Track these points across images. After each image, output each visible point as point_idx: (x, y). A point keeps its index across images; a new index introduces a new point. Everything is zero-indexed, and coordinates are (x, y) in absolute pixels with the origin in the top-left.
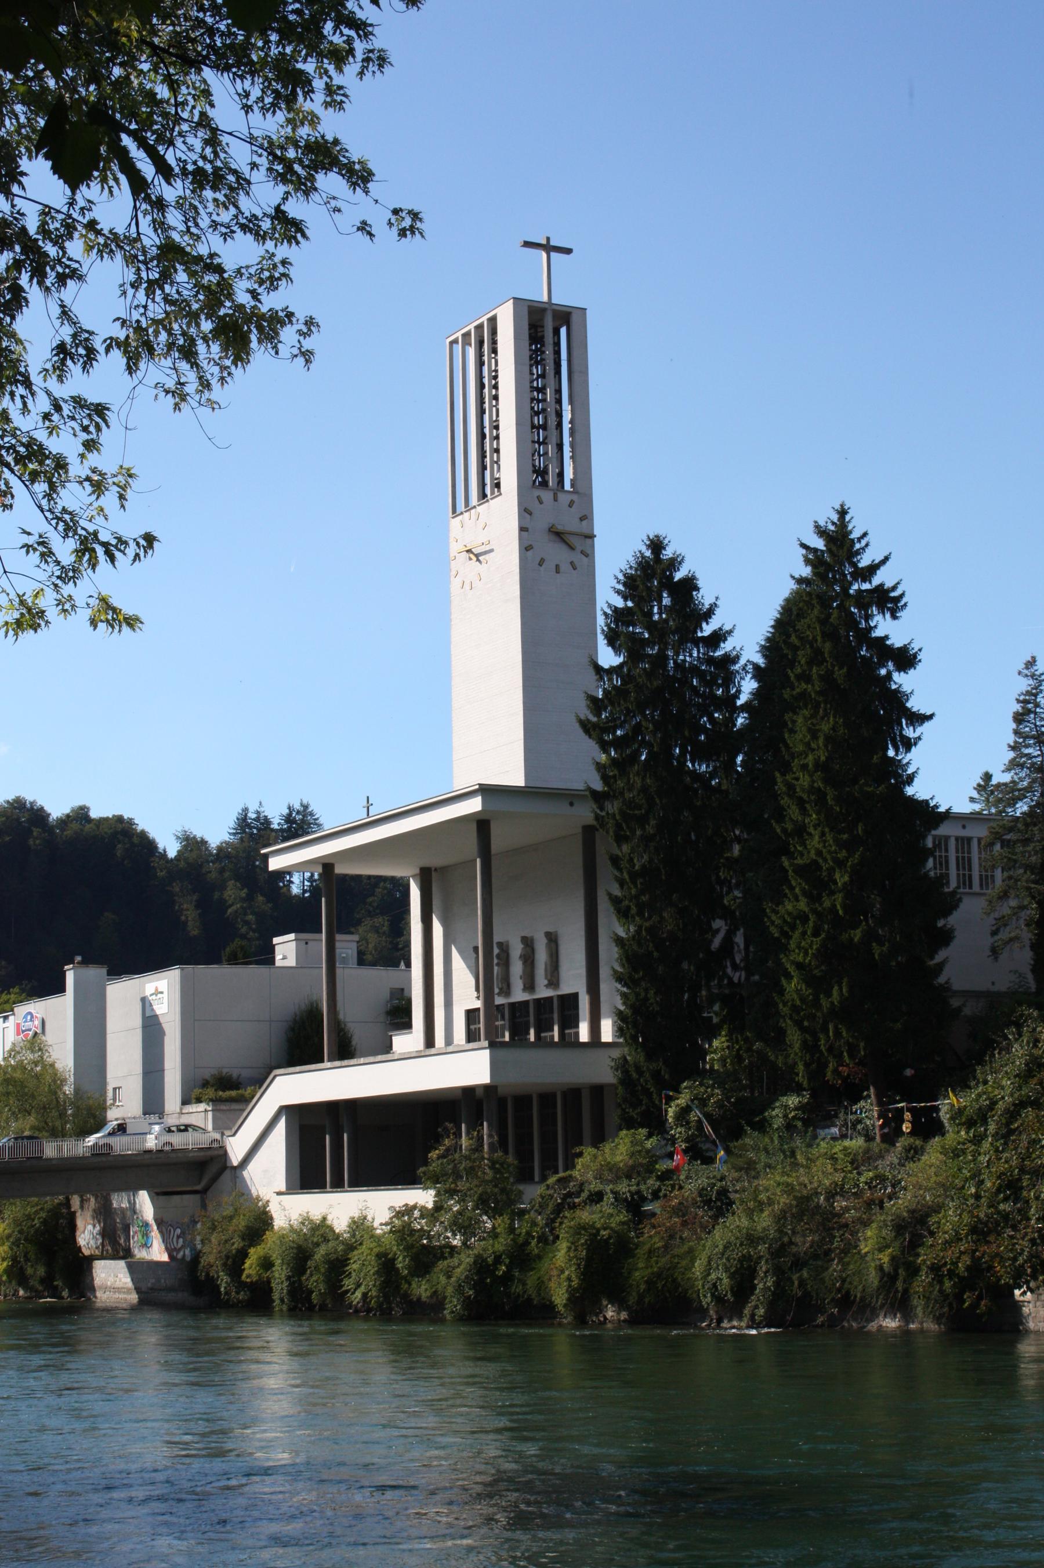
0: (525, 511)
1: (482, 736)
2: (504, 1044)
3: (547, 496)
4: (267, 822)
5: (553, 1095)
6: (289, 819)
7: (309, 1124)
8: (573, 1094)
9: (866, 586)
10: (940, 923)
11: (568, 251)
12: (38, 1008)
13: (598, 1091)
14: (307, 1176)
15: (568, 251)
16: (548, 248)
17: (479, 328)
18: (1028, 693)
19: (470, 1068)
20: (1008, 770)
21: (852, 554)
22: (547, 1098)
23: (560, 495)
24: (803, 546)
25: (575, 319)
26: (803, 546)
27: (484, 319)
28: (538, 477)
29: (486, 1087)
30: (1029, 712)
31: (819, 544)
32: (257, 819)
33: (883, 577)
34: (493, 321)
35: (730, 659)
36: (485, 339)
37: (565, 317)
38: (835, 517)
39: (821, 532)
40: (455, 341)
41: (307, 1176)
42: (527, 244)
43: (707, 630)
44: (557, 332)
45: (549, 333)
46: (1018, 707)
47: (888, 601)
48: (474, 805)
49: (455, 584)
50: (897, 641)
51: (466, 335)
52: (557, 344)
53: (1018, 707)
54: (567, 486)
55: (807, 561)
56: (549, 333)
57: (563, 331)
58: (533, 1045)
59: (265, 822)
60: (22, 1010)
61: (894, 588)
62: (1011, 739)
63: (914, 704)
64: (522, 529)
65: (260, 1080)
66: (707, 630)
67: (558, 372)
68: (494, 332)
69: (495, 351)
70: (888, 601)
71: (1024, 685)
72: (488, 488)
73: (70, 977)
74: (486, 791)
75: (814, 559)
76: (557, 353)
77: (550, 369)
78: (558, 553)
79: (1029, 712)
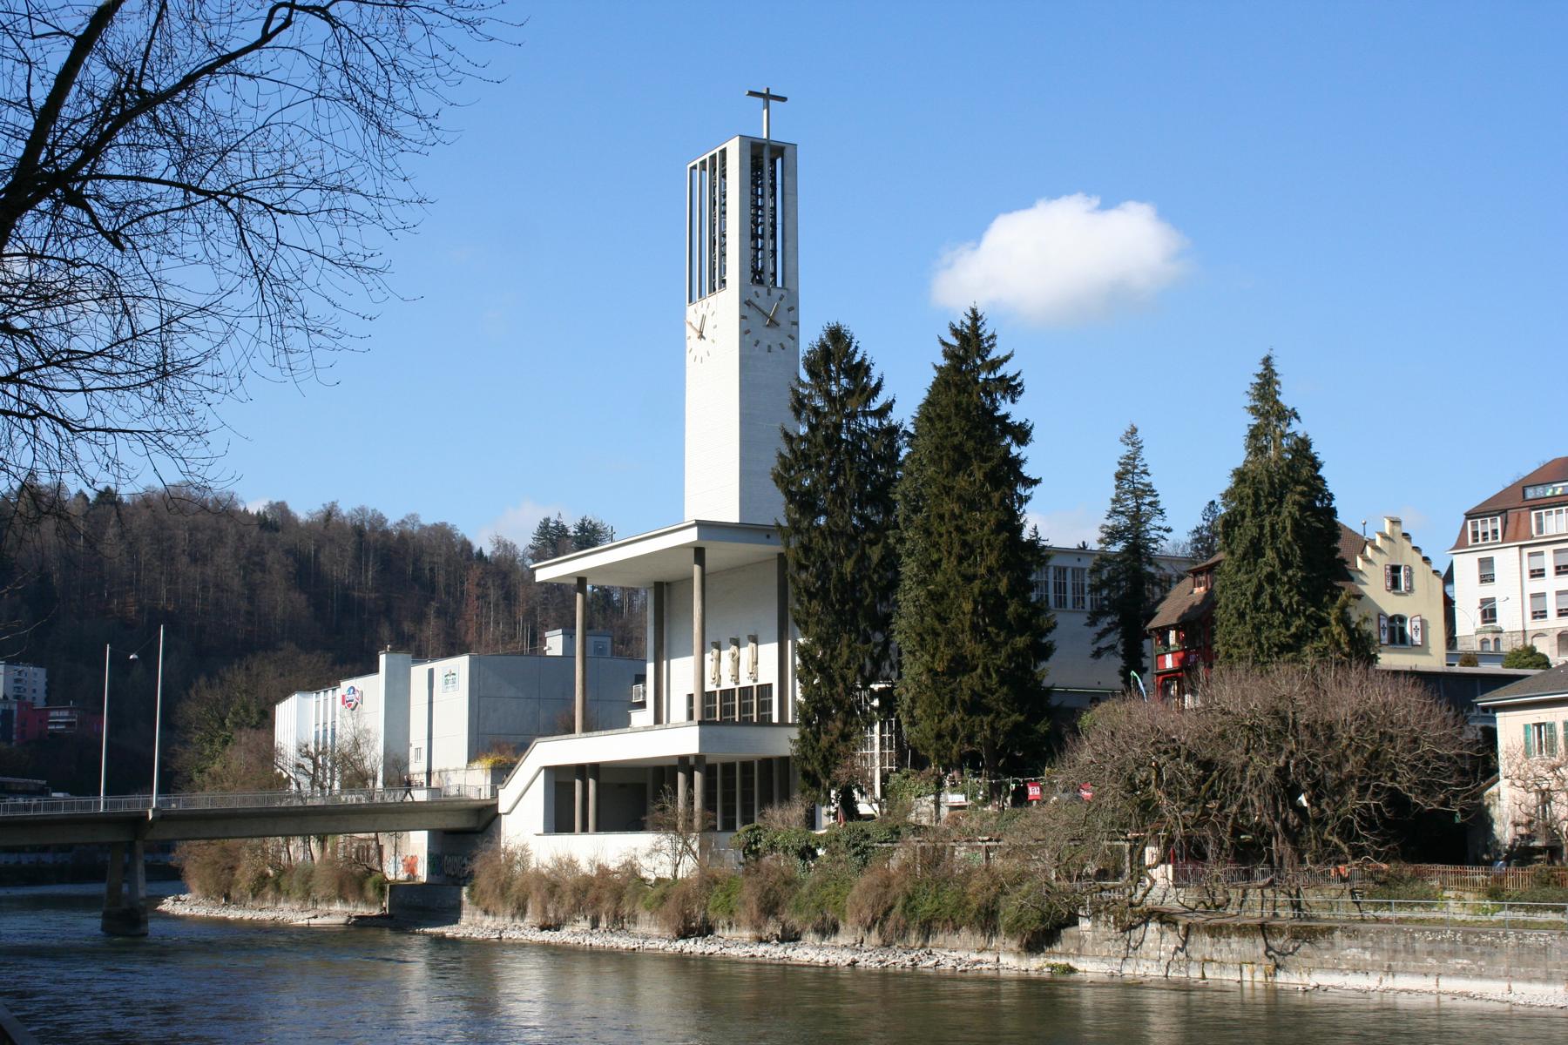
0: (746, 303)
1: (711, 476)
2: (714, 723)
3: (762, 290)
4: (564, 529)
5: (752, 763)
6: (582, 528)
7: (561, 781)
8: (767, 763)
9: (992, 376)
10: (1044, 641)
11: (784, 99)
12: (359, 683)
13: (785, 760)
14: (560, 820)
15: (784, 99)
16: (767, 97)
17: (713, 157)
18: (1128, 457)
19: (682, 740)
20: (1110, 516)
21: (982, 352)
22: (747, 766)
23: (774, 291)
24: (944, 343)
25: (787, 153)
26: (944, 343)
27: (717, 151)
28: (756, 275)
29: (696, 756)
30: (1128, 472)
31: (954, 342)
32: (556, 528)
33: (1007, 370)
34: (723, 152)
35: (892, 431)
36: (717, 165)
37: (779, 150)
38: (968, 322)
39: (956, 333)
40: (695, 167)
41: (560, 820)
42: (752, 93)
43: (875, 405)
44: (773, 162)
45: (766, 162)
46: (1119, 468)
47: (1011, 388)
48: (691, 536)
49: (689, 358)
50: (1016, 418)
51: (704, 163)
52: (774, 172)
53: (1119, 468)
54: (779, 284)
55: (946, 355)
56: (766, 162)
57: (779, 161)
58: (738, 724)
59: (562, 530)
60: (345, 685)
61: (1014, 378)
62: (1112, 493)
63: (1026, 470)
64: (742, 317)
65: (522, 749)
66: (875, 405)
67: (774, 194)
68: (723, 164)
69: (724, 176)
70: (1011, 388)
71: (1125, 450)
72: (717, 282)
73: (382, 658)
74: (701, 525)
75: (949, 352)
76: (774, 178)
77: (768, 191)
78: (770, 337)
79: (1128, 472)
